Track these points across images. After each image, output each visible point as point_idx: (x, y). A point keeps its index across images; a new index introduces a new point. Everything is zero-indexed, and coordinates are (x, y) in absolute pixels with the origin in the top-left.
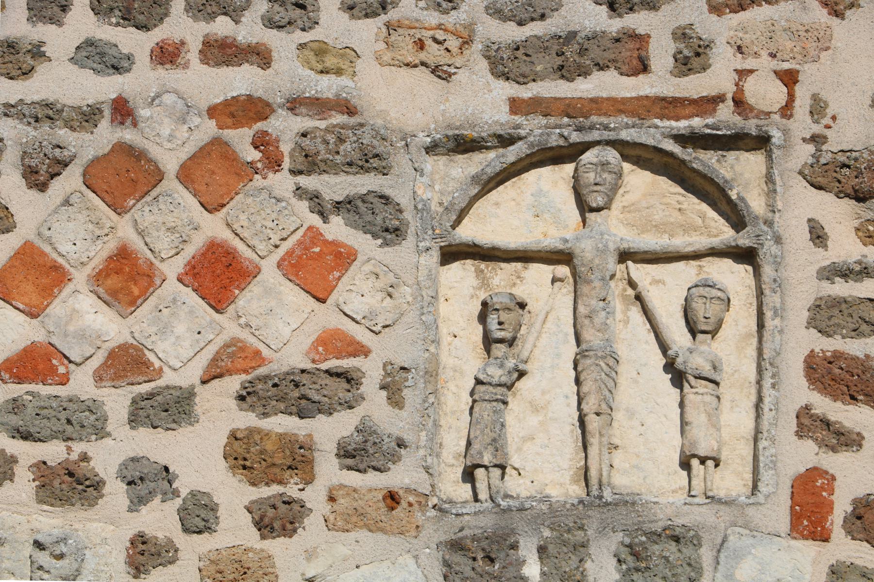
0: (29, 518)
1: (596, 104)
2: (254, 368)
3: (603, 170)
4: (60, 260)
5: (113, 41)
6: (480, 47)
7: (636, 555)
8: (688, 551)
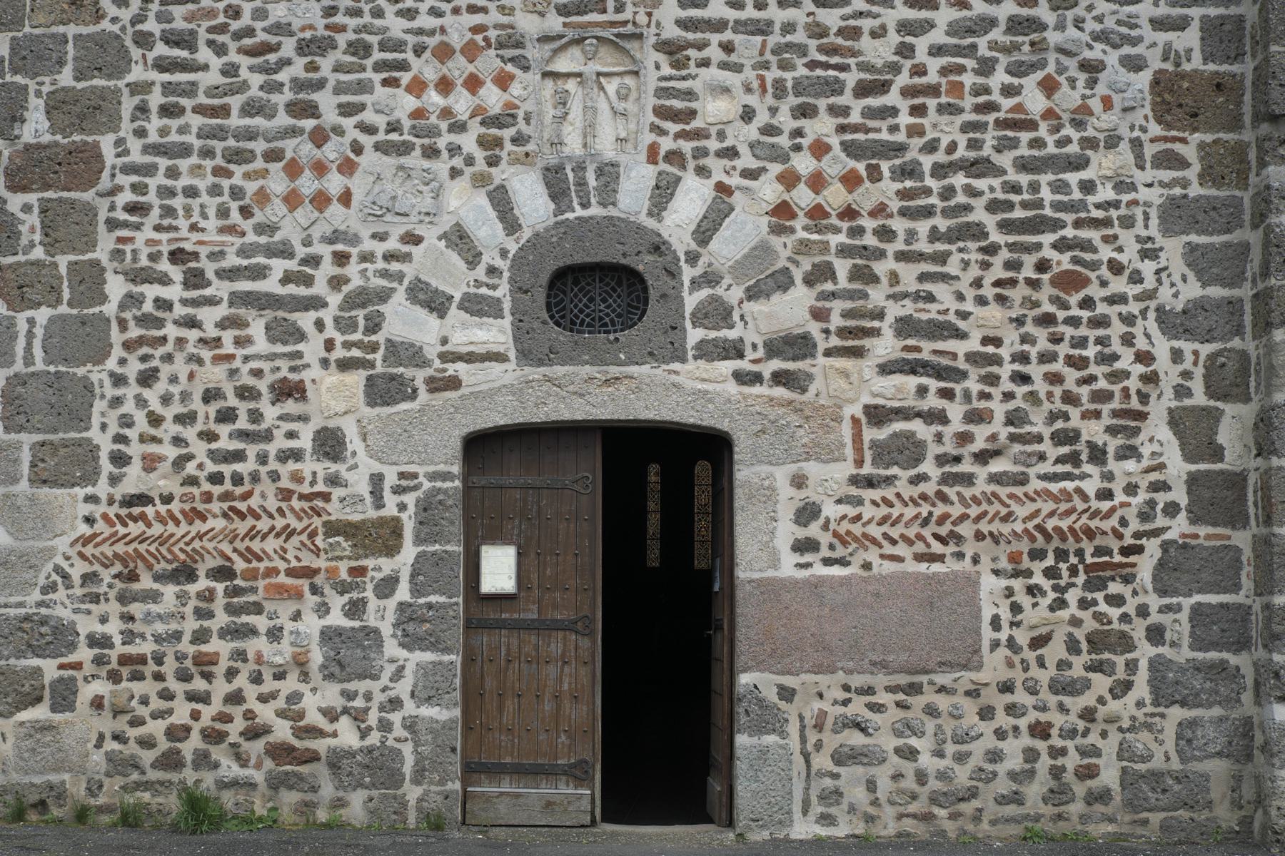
1: (591, 24)
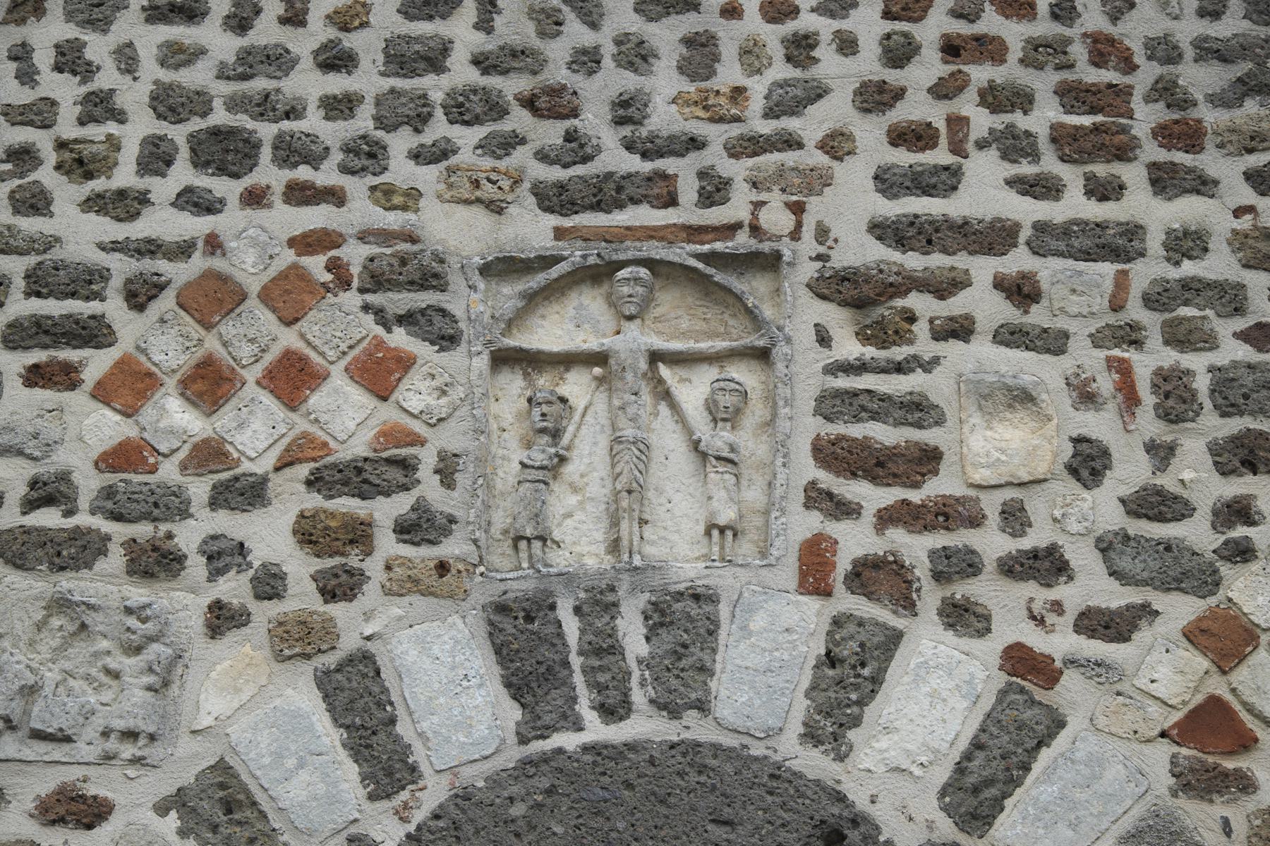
0: (120, 588)
1: (631, 232)
2: (322, 457)
3: (636, 284)
4: (154, 369)
5: (208, 187)
6: (529, 186)
7: (663, 613)
8: (708, 608)
